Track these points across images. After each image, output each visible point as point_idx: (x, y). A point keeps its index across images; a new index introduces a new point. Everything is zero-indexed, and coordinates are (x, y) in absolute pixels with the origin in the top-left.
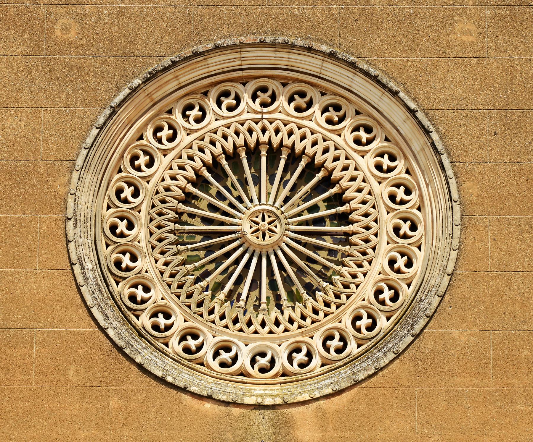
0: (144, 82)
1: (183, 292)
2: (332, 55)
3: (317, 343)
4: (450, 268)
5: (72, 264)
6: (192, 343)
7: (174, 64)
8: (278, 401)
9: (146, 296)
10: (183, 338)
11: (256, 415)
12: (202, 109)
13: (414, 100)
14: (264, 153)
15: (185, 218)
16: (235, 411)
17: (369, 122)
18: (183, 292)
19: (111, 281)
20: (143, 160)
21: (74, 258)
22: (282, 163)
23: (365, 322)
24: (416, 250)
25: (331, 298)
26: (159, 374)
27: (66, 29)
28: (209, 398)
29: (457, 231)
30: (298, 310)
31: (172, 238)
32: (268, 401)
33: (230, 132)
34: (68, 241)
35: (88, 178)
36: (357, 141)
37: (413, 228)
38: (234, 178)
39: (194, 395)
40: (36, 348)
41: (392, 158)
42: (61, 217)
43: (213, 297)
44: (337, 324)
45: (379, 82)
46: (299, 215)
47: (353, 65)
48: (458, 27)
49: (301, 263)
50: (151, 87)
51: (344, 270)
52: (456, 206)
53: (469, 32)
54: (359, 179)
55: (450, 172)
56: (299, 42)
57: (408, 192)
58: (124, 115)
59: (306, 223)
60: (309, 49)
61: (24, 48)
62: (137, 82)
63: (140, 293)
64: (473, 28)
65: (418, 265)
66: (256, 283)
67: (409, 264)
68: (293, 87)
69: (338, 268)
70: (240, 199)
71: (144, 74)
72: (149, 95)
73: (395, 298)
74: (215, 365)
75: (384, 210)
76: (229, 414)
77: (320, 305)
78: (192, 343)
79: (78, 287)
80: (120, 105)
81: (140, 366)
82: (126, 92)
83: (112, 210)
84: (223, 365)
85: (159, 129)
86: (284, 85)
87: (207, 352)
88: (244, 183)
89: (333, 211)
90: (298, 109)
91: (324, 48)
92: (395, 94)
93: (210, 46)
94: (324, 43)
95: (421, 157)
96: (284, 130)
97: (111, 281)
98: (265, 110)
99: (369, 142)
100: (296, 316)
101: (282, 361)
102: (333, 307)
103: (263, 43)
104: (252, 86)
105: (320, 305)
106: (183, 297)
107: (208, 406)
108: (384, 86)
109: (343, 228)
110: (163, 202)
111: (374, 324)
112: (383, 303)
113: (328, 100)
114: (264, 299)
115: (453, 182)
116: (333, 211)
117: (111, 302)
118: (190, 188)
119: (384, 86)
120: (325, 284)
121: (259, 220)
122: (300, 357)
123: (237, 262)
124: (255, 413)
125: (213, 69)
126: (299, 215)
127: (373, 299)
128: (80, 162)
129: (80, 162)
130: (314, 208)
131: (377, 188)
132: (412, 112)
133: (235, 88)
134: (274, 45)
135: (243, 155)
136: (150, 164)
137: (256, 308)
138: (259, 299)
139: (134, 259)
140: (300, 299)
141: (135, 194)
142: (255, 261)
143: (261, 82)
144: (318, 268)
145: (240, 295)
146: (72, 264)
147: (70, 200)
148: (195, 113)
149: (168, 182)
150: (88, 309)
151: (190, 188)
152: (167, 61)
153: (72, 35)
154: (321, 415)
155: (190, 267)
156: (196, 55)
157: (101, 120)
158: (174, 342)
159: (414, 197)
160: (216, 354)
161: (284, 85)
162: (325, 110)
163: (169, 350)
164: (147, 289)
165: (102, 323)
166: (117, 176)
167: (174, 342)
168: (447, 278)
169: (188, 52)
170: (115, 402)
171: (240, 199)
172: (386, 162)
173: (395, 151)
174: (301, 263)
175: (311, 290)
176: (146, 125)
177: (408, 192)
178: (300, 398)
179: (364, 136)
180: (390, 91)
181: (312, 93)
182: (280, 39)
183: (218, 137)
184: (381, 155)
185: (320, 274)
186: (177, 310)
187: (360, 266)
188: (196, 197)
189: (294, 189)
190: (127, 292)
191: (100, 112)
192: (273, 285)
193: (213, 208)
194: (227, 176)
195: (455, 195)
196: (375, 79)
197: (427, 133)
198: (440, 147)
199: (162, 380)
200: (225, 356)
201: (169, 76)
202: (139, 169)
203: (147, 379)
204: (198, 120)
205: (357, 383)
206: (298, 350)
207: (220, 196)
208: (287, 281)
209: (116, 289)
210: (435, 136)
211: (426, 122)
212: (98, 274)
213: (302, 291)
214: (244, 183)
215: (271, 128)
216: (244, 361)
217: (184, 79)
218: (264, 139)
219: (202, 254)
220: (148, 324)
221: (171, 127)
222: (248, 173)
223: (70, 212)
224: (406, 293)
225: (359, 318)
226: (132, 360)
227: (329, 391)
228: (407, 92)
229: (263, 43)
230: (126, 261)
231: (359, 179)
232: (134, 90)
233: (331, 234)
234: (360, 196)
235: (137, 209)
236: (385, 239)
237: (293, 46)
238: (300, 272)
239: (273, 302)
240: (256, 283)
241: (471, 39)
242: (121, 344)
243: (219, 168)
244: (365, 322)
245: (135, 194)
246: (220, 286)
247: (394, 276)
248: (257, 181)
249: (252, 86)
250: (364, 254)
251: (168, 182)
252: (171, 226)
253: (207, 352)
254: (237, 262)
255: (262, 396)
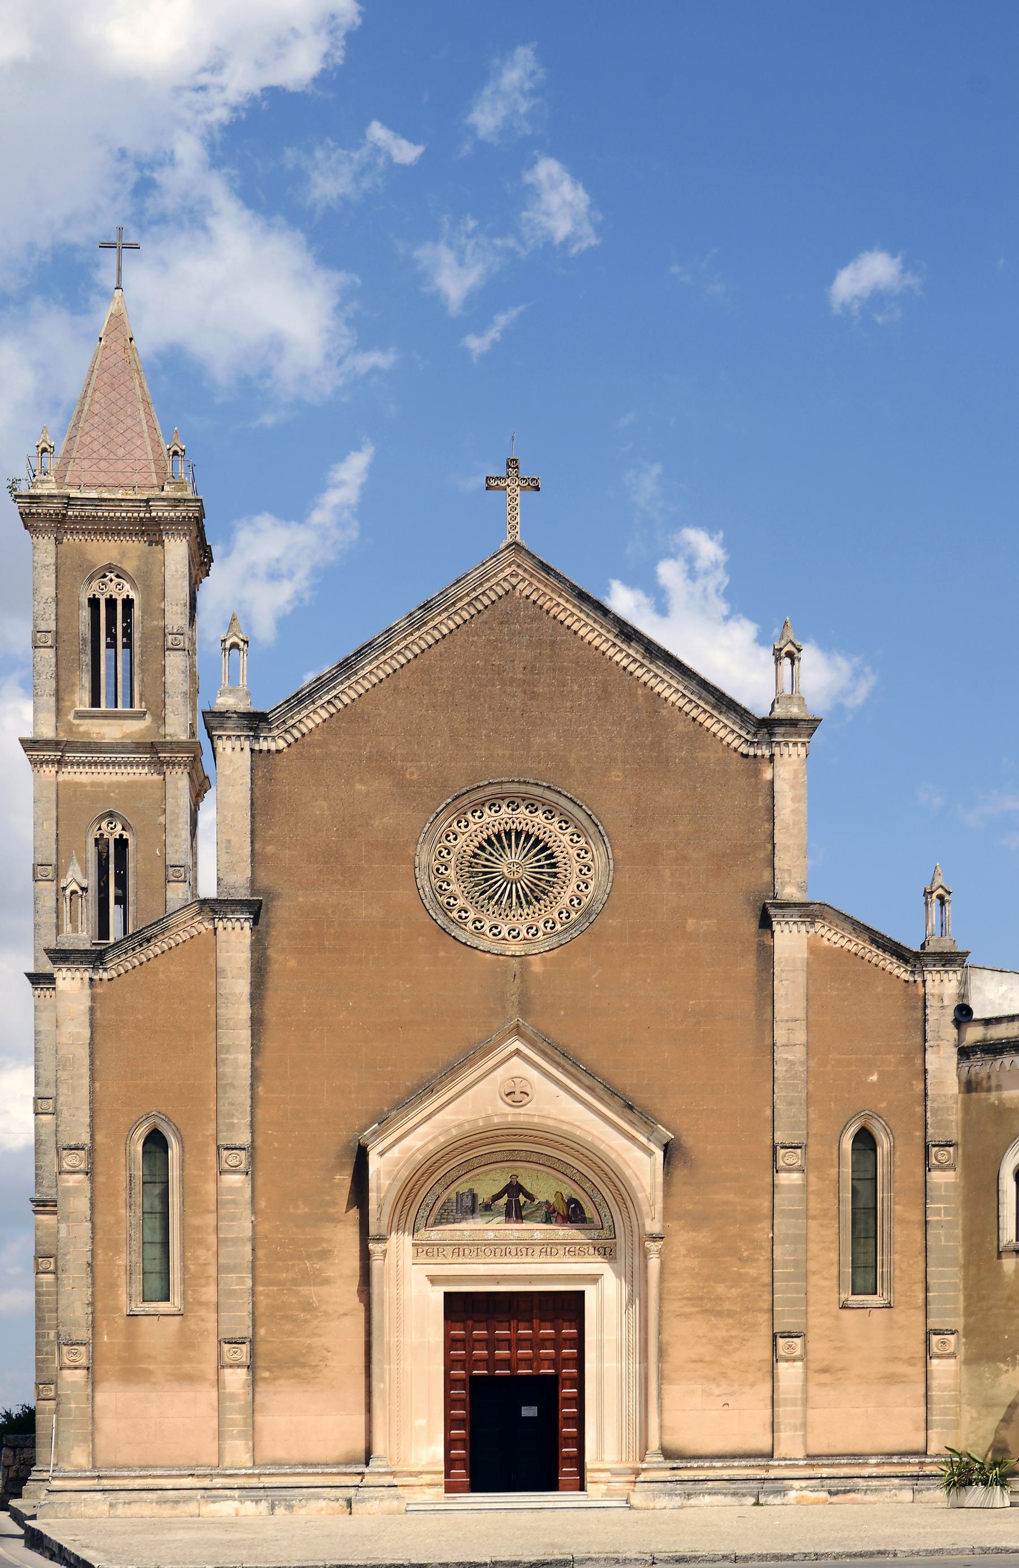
0: (253, 1297)
1: (474, 901)
2: (549, 787)
3: (541, 925)
4: (608, 891)
5: (418, 889)
6: (479, 925)
7: (468, 791)
8: (523, 953)
9: (455, 902)
10: (474, 923)
11: (512, 960)
12: (481, 812)
13: (590, 809)
14: (513, 834)
15: (473, 865)
16: (501, 958)
17: (567, 819)
18: (474, 901)
19: (438, 896)
20: (452, 837)
21: (419, 886)
22: (523, 838)
23: (564, 915)
24: (590, 880)
25: (548, 903)
26: (464, 941)
27: (412, 774)
28: (489, 952)
29: (611, 873)
30: (532, 910)
31: (468, 875)
32: (518, 954)
33: (496, 823)
34: (416, 878)
35: (425, 847)
36: (561, 828)
37: (589, 870)
38: (498, 846)
39: (480, 950)
40: (402, 928)
41: (579, 836)
42: (412, 866)
43: (489, 903)
44: (551, 916)
45: (572, 801)
46: (531, 863)
47: (559, 792)
48: (613, 774)
49: (533, 887)
50: (456, 802)
51: (555, 891)
52: (611, 861)
53: (618, 776)
54: (562, 847)
55: (608, 845)
56: (532, 781)
57: (586, 853)
58: (442, 816)
59: (535, 867)
60: (537, 784)
61: (391, 783)
62: (449, 800)
63: (452, 901)
64: (620, 774)
65: (591, 888)
66: (510, 896)
67: (587, 887)
68: (528, 802)
69: (551, 889)
70: (501, 856)
71: (453, 797)
72: (455, 806)
73: (579, 904)
74: (490, 935)
75: (574, 862)
76: (498, 960)
77: (542, 907)
78: (479, 925)
79: (422, 900)
80: (440, 812)
81: (454, 937)
82: (444, 805)
83: (437, 862)
84: (494, 935)
85: (460, 822)
86: (523, 800)
87: (486, 929)
88: (503, 848)
89: (548, 862)
90: (531, 812)
91: (544, 784)
92: (581, 807)
93: (486, 783)
94: (544, 781)
95: (593, 837)
96: (524, 823)
97: (438, 896)
98: (514, 813)
99: (567, 828)
100: (530, 912)
101: (523, 933)
102: (549, 908)
103: (513, 781)
104: (507, 801)
105: (542, 907)
106: (474, 903)
107: (488, 955)
108: (575, 803)
109: (554, 870)
110: (465, 851)
111: (569, 916)
112: (573, 906)
113: (546, 808)
114: (514, 904)
115: (609, 850)
116: (548, 862)
117: (438, 906)
118: (477, 851)
119: (575, 803)
120: (545, 897)
121: (511, 866)
122: (533, 931)
123: (500, 886)
124: (511, 958)
125: (487, 793)
126: (531, 863)
127: (568, 904)
128: (421, 840)
129: (421, 840)
130: (539, 861)
131: (570, 851)
132: (590, 816)
133: (498, 802)
134: (518, 782)
135: (503, 835)
136: (455, 839)
137: (510, 908)
138: (511, 903)
139: (448, 885)
140: (532, 904)
141: (449, 853)
142: (509, 886)
143: (512, 799)
144: (541, 889)
145: (502, 902)
146: (418, 889)
147: (417, 858)
148: (478, 814)
149: (465, 848)
150: (428, 911)
151: (477, 851)
152: (464, 790)
153: (415, 777)
154: (544, 959)
155: (476, 888)
156: (479, 787)
157: (432, 819)
158: (470, 924)
159: (589, 855)
160: (491, 930)
161: (523, 800)
162: (544, 813)
163: (467, 928)
164: (455, 899)
165: (434, 917)
166: (439, 845)
167: (470, 924)
168: (606, 896)
169: (475, 786)
170: (442, 954)
171: (501, 856)
172: (575, 838)
173: (580, 833)
174: (533, 887)
175: (538, 899)
176: (453, 820)
177: (586, 853)
178: (533, 952)
179: (564, 826)
180: (578, 805)
181: (537, 804)
182: (522, 780)
183: (490, 826)
184: (573, 835)
185: (542, 892)
186: (471, 909)
187: (562, 888)
188: (479, 855)
189: (529, 851)
190: (445, 901)
191: (431, 815)
192: (518, 897)
193: (487, 860)
194: (494, 844)
195: (611, 856)
196: (571, 799)
197: (597, 826)
198: (603, 833)
199: (465, 944)
200: (495, 931)
201: (465, 797)
202: (449, 841)
203: (457, 943)
204: (480, 817)
205: (562, 945)
206: (531, 928)
207: (491, 854)
208: (525, 895)
209: (440, 899)
210: (601, 828)
211: (596, 821)
212: (431, 892)
213: (533, 900)
214: (503, 848)
215: (517, 822)
216: (505, 933)
217: (472, 798)
218: (514, 827)
219: (483, 882)
220: (457, 916)
221: (466, 821)
222: (505, 843)
223: (417, 864)
224: (585, 901)
225: (561, 913)
226: (450, 935)
227: (547, 949)
228: (586, 806)
229: (513, 781)
230: (445, 886)
231: (562, 847)
232: (448, 805)
233: (548, 873)
234: (562, 855)
235: (450, 861)
236: (575, 876)
237: (528, 783)
238: (532, 891)
239: (518, 905)
240: (510, 896)
241: (619, 779)
242: (445, 927)
243: (861, 1204)
244: (564, 915)
245: (449, 853)
246: (491, 898)
247: (579, 893)
248: (510, 846)
249: (507, 801)
250: (564, 882)
251: (465, 848)
252: (467, 869)
253: (486, 929)
254: (500, 886)
255: (515, 951)
